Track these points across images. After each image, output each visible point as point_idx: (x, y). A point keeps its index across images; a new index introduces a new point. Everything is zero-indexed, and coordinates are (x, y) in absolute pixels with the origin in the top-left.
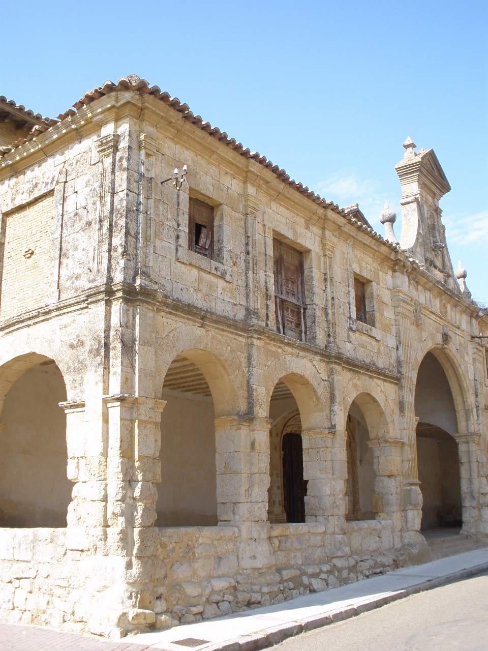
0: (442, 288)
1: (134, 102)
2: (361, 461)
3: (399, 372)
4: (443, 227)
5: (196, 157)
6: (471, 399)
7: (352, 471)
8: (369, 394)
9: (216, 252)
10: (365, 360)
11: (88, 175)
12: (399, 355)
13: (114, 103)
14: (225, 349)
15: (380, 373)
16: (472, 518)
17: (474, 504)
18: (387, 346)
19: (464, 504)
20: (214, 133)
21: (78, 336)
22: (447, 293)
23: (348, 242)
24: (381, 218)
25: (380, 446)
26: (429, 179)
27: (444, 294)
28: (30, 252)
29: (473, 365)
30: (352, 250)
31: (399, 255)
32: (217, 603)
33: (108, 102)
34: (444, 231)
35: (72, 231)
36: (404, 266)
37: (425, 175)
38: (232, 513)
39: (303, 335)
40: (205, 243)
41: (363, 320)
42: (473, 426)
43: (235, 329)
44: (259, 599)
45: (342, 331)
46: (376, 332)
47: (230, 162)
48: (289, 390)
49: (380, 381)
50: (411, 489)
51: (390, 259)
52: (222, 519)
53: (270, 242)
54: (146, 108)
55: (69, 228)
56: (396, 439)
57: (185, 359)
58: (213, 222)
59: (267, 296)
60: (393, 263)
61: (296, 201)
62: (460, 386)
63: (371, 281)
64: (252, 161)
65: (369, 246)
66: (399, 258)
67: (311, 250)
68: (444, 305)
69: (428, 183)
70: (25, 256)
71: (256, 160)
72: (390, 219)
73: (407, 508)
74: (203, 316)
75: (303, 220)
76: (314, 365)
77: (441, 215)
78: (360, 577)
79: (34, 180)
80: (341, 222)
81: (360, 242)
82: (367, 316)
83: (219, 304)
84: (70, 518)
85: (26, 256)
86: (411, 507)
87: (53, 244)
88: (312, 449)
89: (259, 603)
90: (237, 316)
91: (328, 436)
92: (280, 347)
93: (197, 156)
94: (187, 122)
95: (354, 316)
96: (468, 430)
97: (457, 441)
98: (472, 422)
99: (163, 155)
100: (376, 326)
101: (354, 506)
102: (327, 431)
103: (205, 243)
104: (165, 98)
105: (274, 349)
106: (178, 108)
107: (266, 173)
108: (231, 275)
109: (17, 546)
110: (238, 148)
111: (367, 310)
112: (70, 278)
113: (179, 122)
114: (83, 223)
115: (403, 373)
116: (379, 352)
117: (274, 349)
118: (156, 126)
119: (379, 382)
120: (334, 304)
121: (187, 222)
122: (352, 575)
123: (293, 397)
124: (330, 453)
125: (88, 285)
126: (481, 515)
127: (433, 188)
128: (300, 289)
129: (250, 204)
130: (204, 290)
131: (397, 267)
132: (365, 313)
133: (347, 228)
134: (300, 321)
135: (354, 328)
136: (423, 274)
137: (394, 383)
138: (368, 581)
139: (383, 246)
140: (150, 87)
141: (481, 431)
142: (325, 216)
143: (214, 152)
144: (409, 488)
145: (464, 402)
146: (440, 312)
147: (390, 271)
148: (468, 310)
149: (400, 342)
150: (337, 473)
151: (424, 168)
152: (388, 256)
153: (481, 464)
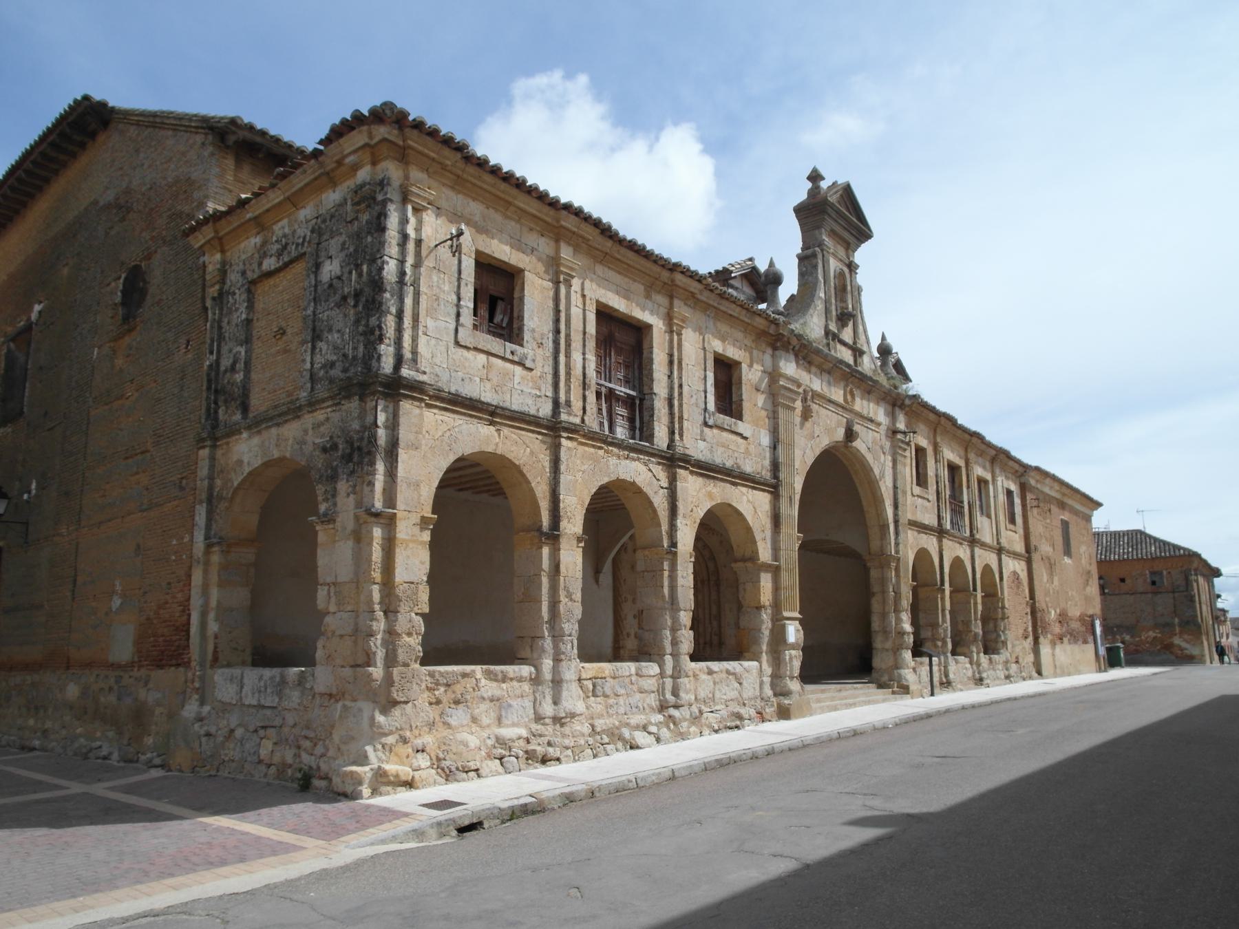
1: (392, 138)
4: (859, 289)
5: (486, 210)
8: (730, 505)
9: (516, 331)
10: (725, 462)
11: (344, 236)
13: (366, 140)
14: (522, 452)
15: (750, 481)
20: (509, 178)
21: (331, 437)
23: (708, 313)
26: (839, 224)
28: (281, 331)
32: (501, 759)
33: (358, 138)
34: (859, 294)
35: (326, 308)
38: (529, 650)
39: (637, 431)
40: (502, 320)
43: (536, 427)
44: (558, 754)
45: (692, 426)
46: (742, 427)
47: (535, 216)
51: (769, 333)
52: (519, 657)
53: (591, 317)
54: (410, 147)
55: (323, 303)
57: (478, 465)
58: (512, 293)
64: (564, 213)
65: (737, 318)
66: (781, 331)
67: (740, 363)
70: (275, 336)
71: (569, 212)
74: (493, 414)
75: (642, 288)
76: (650, 470)
77: (857, 271)
78: (706, 731)
79: (283, 240)
80: (695, 288)
81: (724, 312)
83: (515, 396)
84: (320, 654)
85: (277, 337)
87: (305, 323)
88: (648, 572)
89: (558, 759)
90: (540, 410)
91: (665, 556)
93: (488, 208)
94: (469, 164)
95: (711, 406)
99: (438, 208)
103: (502, 320)
104: (433, 133)
106: (454, 146)
108: (534, 361)
109: (263, 689)
110: (542, 197)
111: (734, 400)
112: (324, 366)
113: (458, 164)
114: (337, 297)
116: (747, 452)
118: (427, 171)
119: (744, 490)
121: (472, 295)
122: (693, 729)
123: (625, 509)
125: (342, 376)
127: (846, 235)
128: (637, 374)
129: (562, 269)
130: (495, 380)
131: (778, 344)
132: (731, 403)
133: (705, 296)
134: (635, 415)
135: (711, 422)
136: (818, 352)
138: (716, 736)
140: (411, 118)
142: (673, 281)
143: (510, 203)
148: (889, 398)
152: (766, 329)
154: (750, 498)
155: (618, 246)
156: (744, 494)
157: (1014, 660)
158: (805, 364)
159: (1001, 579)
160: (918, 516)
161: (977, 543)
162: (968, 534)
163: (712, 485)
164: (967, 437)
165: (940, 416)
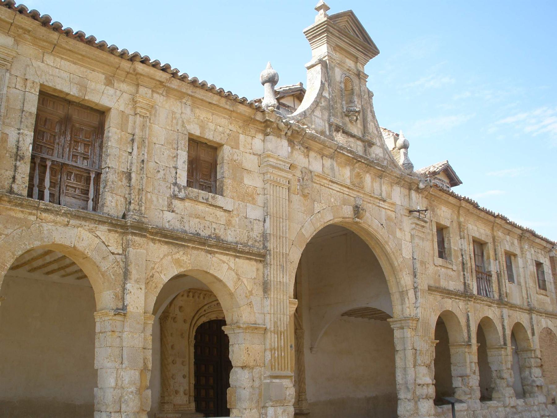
0: (349, 155)
2: (311, 349)
3: (265, 247)
6: (406, 280)
7: (298, 359)
12: (266, 227)
16: (407, 411)
17: (409, 396)
18: (246, 218)
19: (399, 397)
22: (361, 162)
23: (184, 101)
24: (261, 80)
25: (234, 333)
26: (344, 41)
27: (356, 163)
29: (411, 242)
30: (192, 111)
31: (267, 115)
36: (279, 129)
37: (336, 36)
41: (213, 189)
42: (408, 310)
48: (74, 263)
49: (228, 257)
50: (271, 382)
51: (257, 120)
56: (255, 324)
59: (17, 157)
60: (263, 125)
61: (84, 53)
62: (391, 265)
63: (223, 145)
65: (218, 106)
66: (267, 118)
68: (358, 175)
69: (342, 45)
72: (269, 79)
73: (267, 405)
82: (217, 184)
86: (271, 403)
88: (102, 333)
91: (114, 318)
92: (30, 214)
96: (403, 314)
97: (392, 326)
98: (407, 305)
100: (225, 195)
101: (299, 396)
102: (112, 313)
105: (20, 215)
107: (22, 20)
115: (268, 248)
117: (20, 215)
120: (143, 168)
124: (118, 339)
126: (417, 409)
131: (268, 130)
137: (256, 260)
139: (241, 105)
141: (419, 315)
142: (135, 70)
144: (269, 381)
145: (398, 283)
146: (351, 182)
147: (260, 135)
149: (267, 213)
150: (126, 363)
151: (334, 28)
152: (253, 117)
153: (418, 352)
154: (232, 265)
155: (65, 37)
156: (224, 262)
157: (551, 401)
158: (302, 148)
159: (533, 334)
160: (441, 283)
161: (534, 310)
162: (496, 296)
163: (181, 253)
164: (492, 219)
165: (460, 200)
